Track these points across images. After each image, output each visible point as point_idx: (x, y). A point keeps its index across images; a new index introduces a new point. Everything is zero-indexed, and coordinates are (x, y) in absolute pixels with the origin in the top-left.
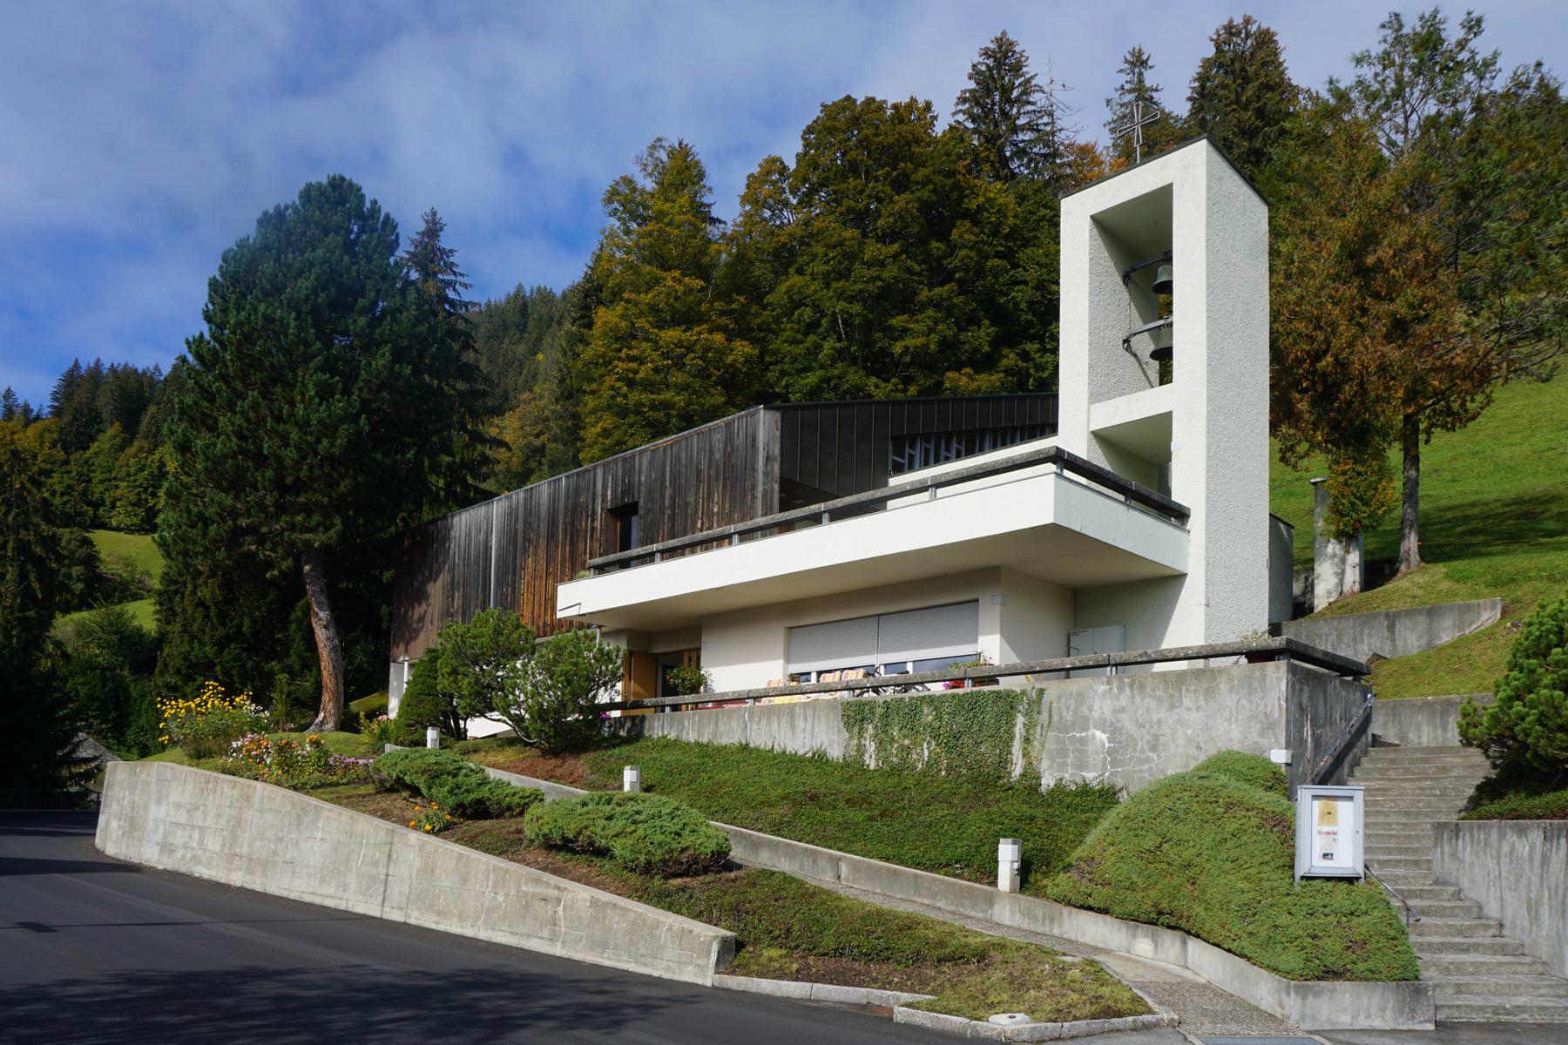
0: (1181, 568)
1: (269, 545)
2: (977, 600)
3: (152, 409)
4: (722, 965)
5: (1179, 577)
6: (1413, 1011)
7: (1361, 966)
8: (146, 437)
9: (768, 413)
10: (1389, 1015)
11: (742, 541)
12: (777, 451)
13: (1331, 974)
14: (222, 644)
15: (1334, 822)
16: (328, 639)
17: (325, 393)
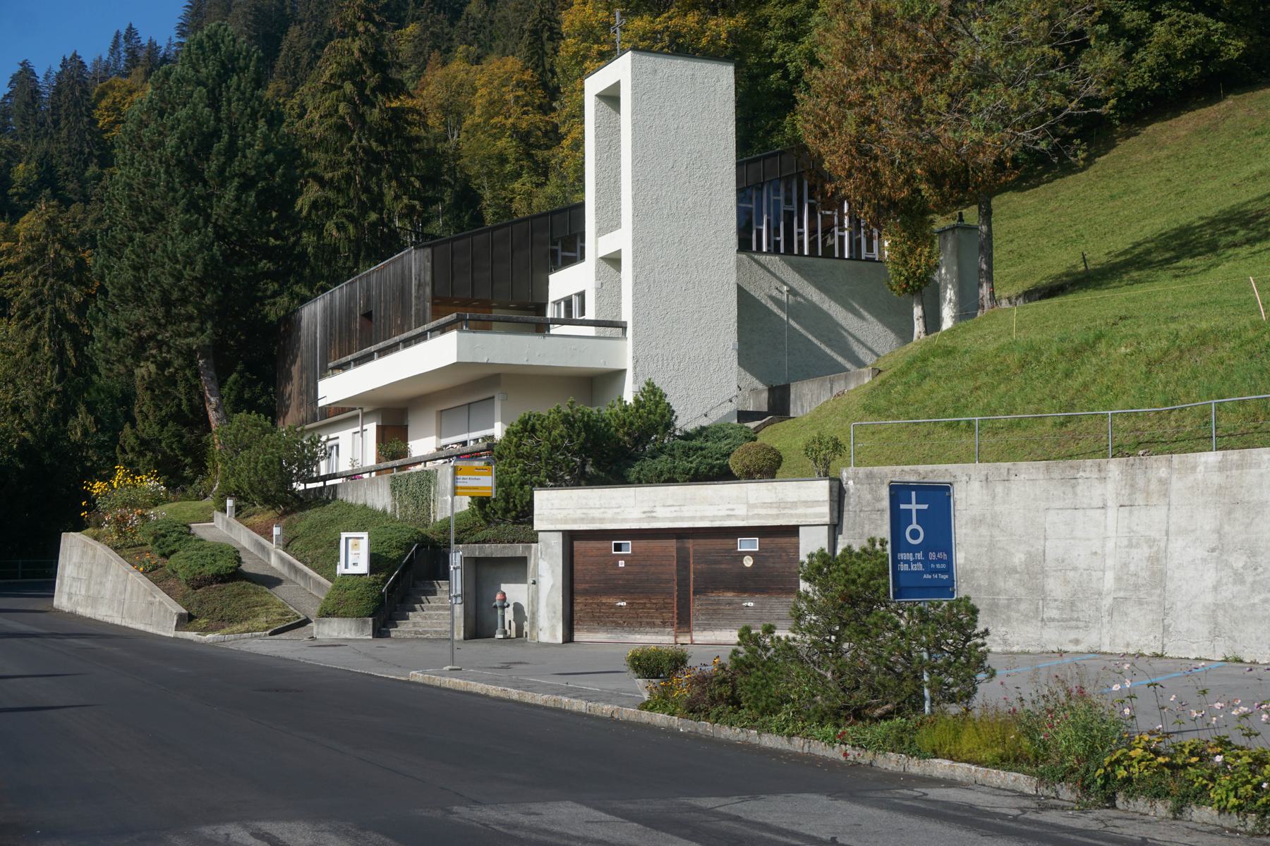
0: (621, 367)
1: (165, 349)
2: (493, 397)
3: (294, 31)
4: (178, 628)
5: (624, 371)
6: (363, 630)
7: (341, 611)
8: (283, 75)
9: (418, 252)
10: (353, 632)
11: (380, 357)
12: (428, 278)
13: (328, 615)
14: (163, 424)
15: (358, 549)
16: (217, 419)
17: (187, 229)
